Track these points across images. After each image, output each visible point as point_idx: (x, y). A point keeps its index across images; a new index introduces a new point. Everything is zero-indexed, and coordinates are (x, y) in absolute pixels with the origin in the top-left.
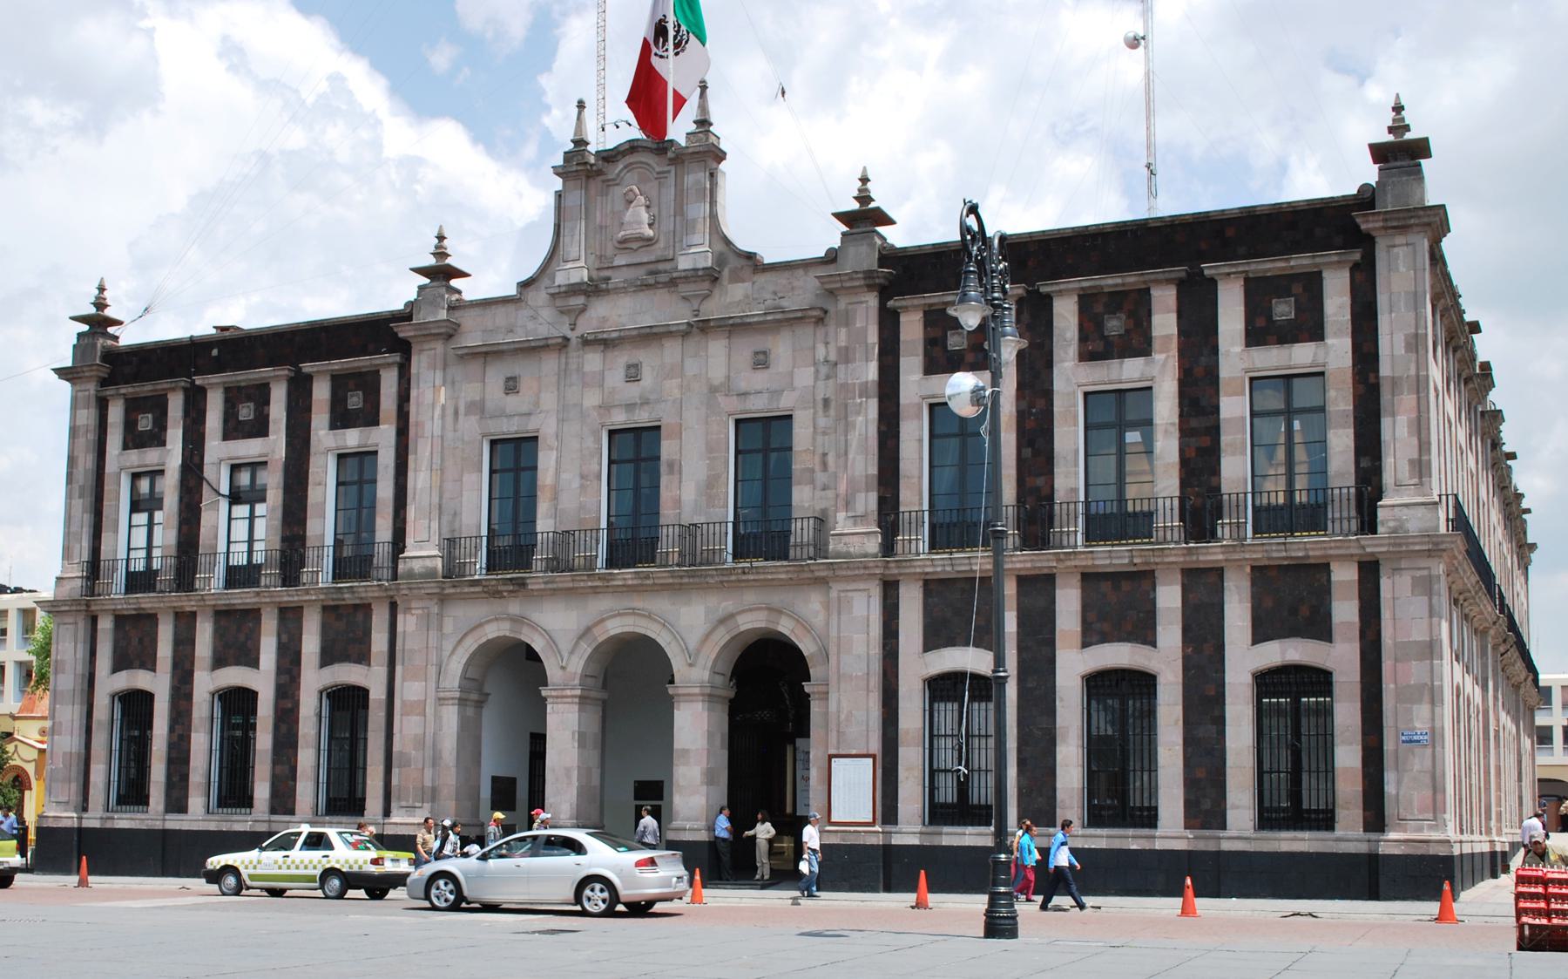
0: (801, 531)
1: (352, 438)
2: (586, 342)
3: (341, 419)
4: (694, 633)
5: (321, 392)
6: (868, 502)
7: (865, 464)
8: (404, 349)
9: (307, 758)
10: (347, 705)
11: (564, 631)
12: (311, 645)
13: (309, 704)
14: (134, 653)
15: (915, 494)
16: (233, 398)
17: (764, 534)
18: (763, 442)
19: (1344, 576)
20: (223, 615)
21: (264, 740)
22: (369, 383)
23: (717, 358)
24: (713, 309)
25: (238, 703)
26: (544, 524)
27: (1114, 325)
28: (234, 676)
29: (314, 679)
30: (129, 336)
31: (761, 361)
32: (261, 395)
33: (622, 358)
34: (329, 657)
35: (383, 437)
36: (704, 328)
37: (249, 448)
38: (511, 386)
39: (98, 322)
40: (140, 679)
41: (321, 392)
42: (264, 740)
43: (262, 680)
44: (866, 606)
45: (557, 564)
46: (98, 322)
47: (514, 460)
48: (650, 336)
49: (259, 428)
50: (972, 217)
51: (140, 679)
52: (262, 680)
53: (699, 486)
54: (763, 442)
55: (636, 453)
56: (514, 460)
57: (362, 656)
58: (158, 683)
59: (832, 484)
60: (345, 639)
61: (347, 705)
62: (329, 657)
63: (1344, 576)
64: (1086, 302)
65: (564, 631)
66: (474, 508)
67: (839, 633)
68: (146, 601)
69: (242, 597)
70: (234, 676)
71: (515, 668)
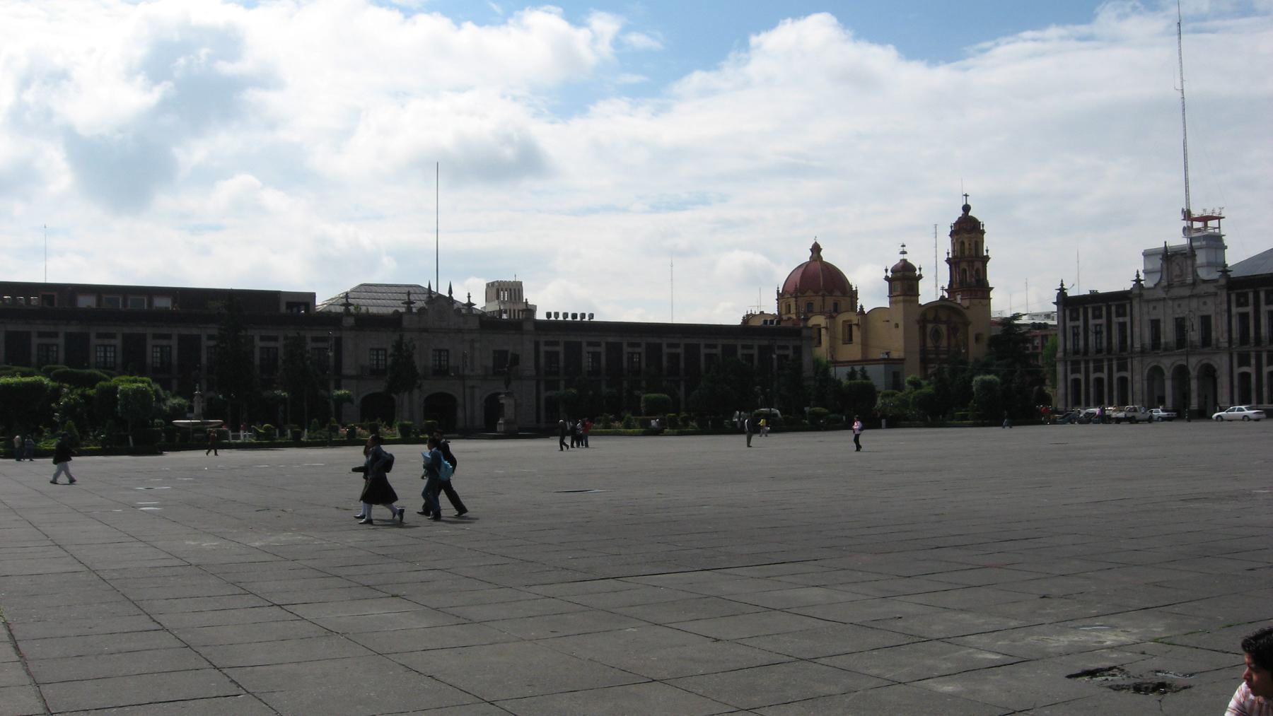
0: (1214, 342)
1: (1121, 319)
2: (1171, 299)
3: (1118, 315)
4: (1193, 363)
5: (1113, 309)
6: (1226, 335)
7: (1225, 327)
8: (1131, 300)
9: (1115, 393)
10: (1123, 381)
11: (1167, 364)
12: (1115, 368)
13: (1115, 381)
14: (1244, 360)
15: (1235, 335)
16: (1094, 309)
17: (1206, 340)
18: (1206, 321)
19: (1253, 354)
20: (1095, 361)
21: (1106, 390)
22: (1124, 306)
23: (1194, 303)
24: (1195, 292)
25: (1099, 381)
26: (1163, 341)
27: (1242, 300)
28: (1098, 375)
29: (1116, 375)
30: (1070, 294)
31: (1205, 303)
32: (1100, 309)
33: (1177, 303)
34: (1119, 370)
35: (1127, 319)
36: (1191, 297)
37: (1098, 321)
38: (1154, 308)
39: (1062, 291)
40: (1077, 376)
41: (1113, 309)
42: (1106, 390)
43: (1105, 375)
44: (1226, 358)
45: (1166, 350)
46: (1062, 291)
47: (1155, 325)
48: (1182, 298)
49: (1100, 317)
50: (59, 480)
51: (1077, 376)
52: (1081, 377)
53: (1168, 334)
54: (1206, 321)
55: (1180, 325)
56: (1155, 325)
57: (1126, 370)
58: (1081, 377)
59: (1219, 332)
60: (1122, 367)
61: (1123, 381)
62: (1119, 370)
63: (1253, 354)
64: (1266, 292)
65: (1167, 364)
66: (1147, 339)
67: (1221, 363)
68: (1100, 356)
69: (1100, 356)
70: (1098, 375)
71: (1156, 372)
